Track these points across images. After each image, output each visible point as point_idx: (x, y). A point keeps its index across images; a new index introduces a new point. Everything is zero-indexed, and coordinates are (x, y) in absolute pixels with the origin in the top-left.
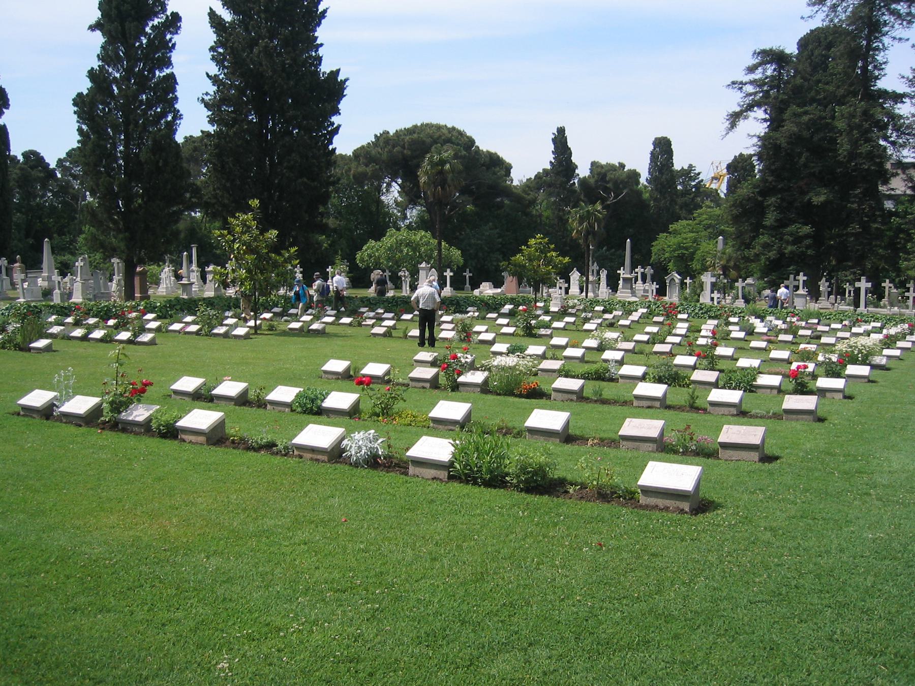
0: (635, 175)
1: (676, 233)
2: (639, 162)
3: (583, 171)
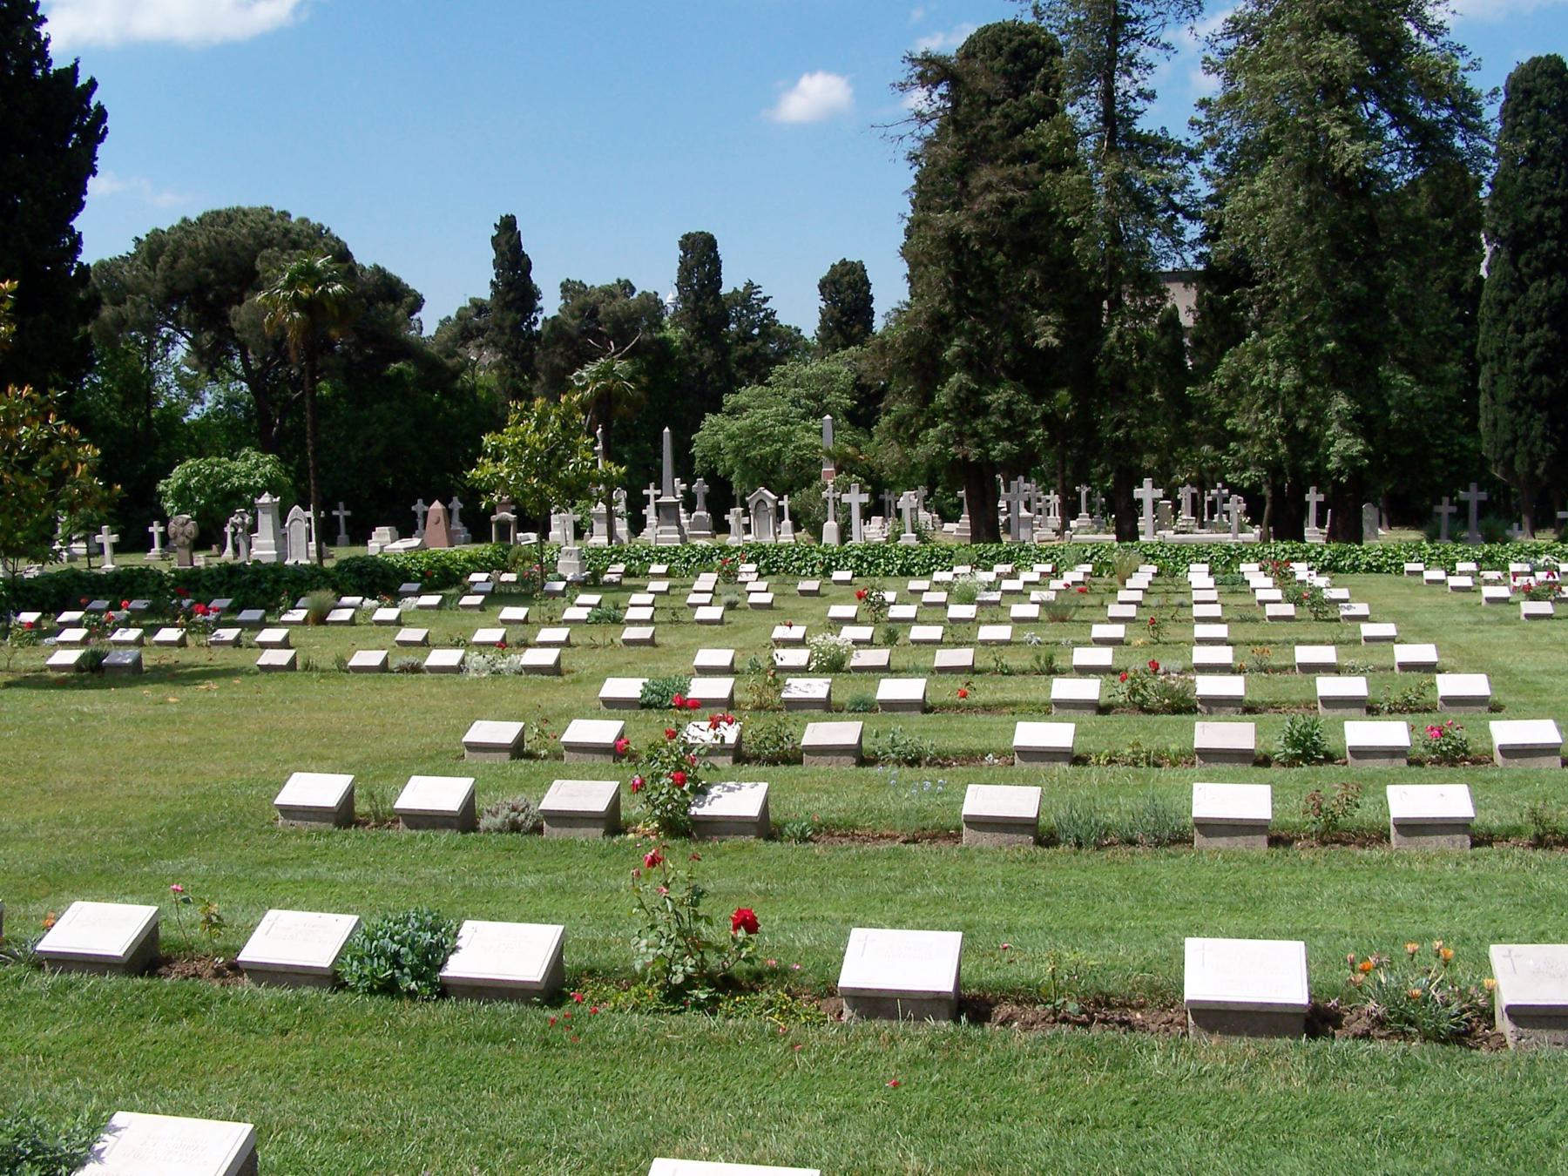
0: (652, 305)
1: (734, 412)
2: (660, 279)
3: (550, 305)
